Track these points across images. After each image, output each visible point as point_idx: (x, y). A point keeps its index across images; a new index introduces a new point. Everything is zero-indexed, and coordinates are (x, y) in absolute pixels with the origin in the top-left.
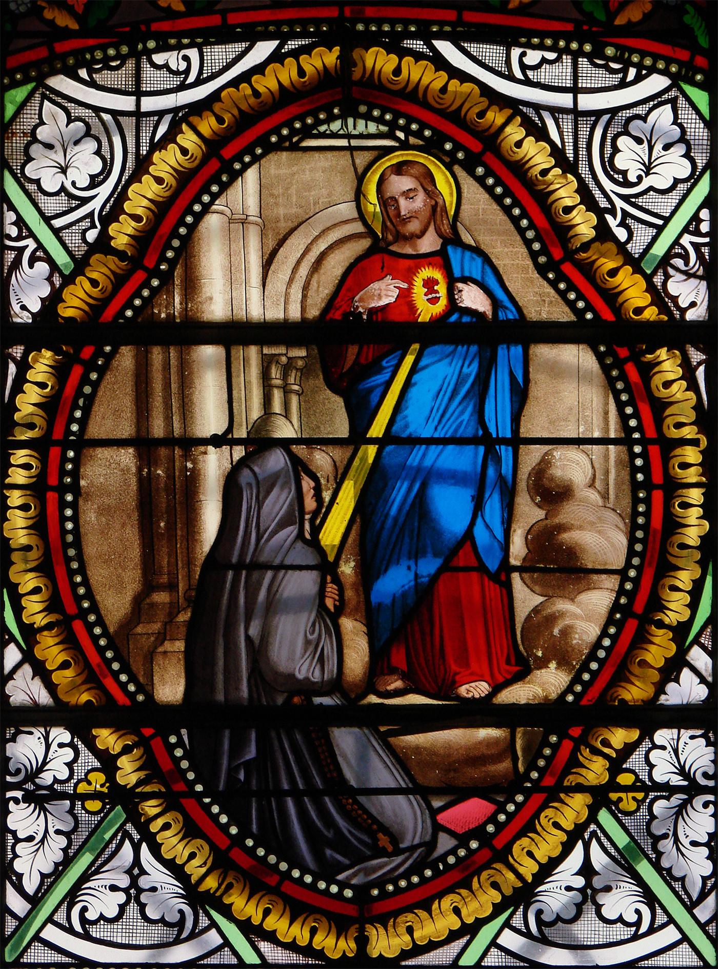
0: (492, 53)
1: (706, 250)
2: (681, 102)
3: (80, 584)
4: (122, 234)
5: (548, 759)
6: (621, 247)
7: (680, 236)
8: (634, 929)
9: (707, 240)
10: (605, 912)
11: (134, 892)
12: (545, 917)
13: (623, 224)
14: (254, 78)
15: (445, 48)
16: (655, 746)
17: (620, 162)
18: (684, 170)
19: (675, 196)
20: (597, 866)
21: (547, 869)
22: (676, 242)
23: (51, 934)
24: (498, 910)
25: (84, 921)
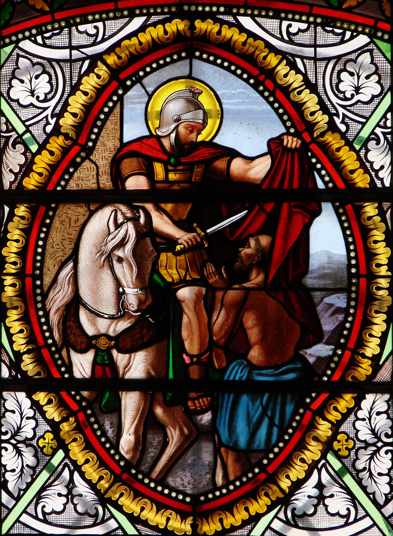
0: (271, 24)
1: (389, 136)
2: (376, 52)
3: (100, 120)
4: (67, 121)
5: (298, 422)
6: (343, 136)
7: (374, 128)
8: (345, 519)
9: (390, 130)
10: (329, 509)
11: (70, 494)
12: (296, 512)
13: (343, 122)
14: (139, 35)
15: (247, 22)
16: (358, 419)
17: (342, 87)
18: (377, 90)
19: (371, 107)
20: (324, 481)
21: (298, 485)
22: (373, 133)
23: (25, 519)
24: (270, 509)
25: (44, 514)
